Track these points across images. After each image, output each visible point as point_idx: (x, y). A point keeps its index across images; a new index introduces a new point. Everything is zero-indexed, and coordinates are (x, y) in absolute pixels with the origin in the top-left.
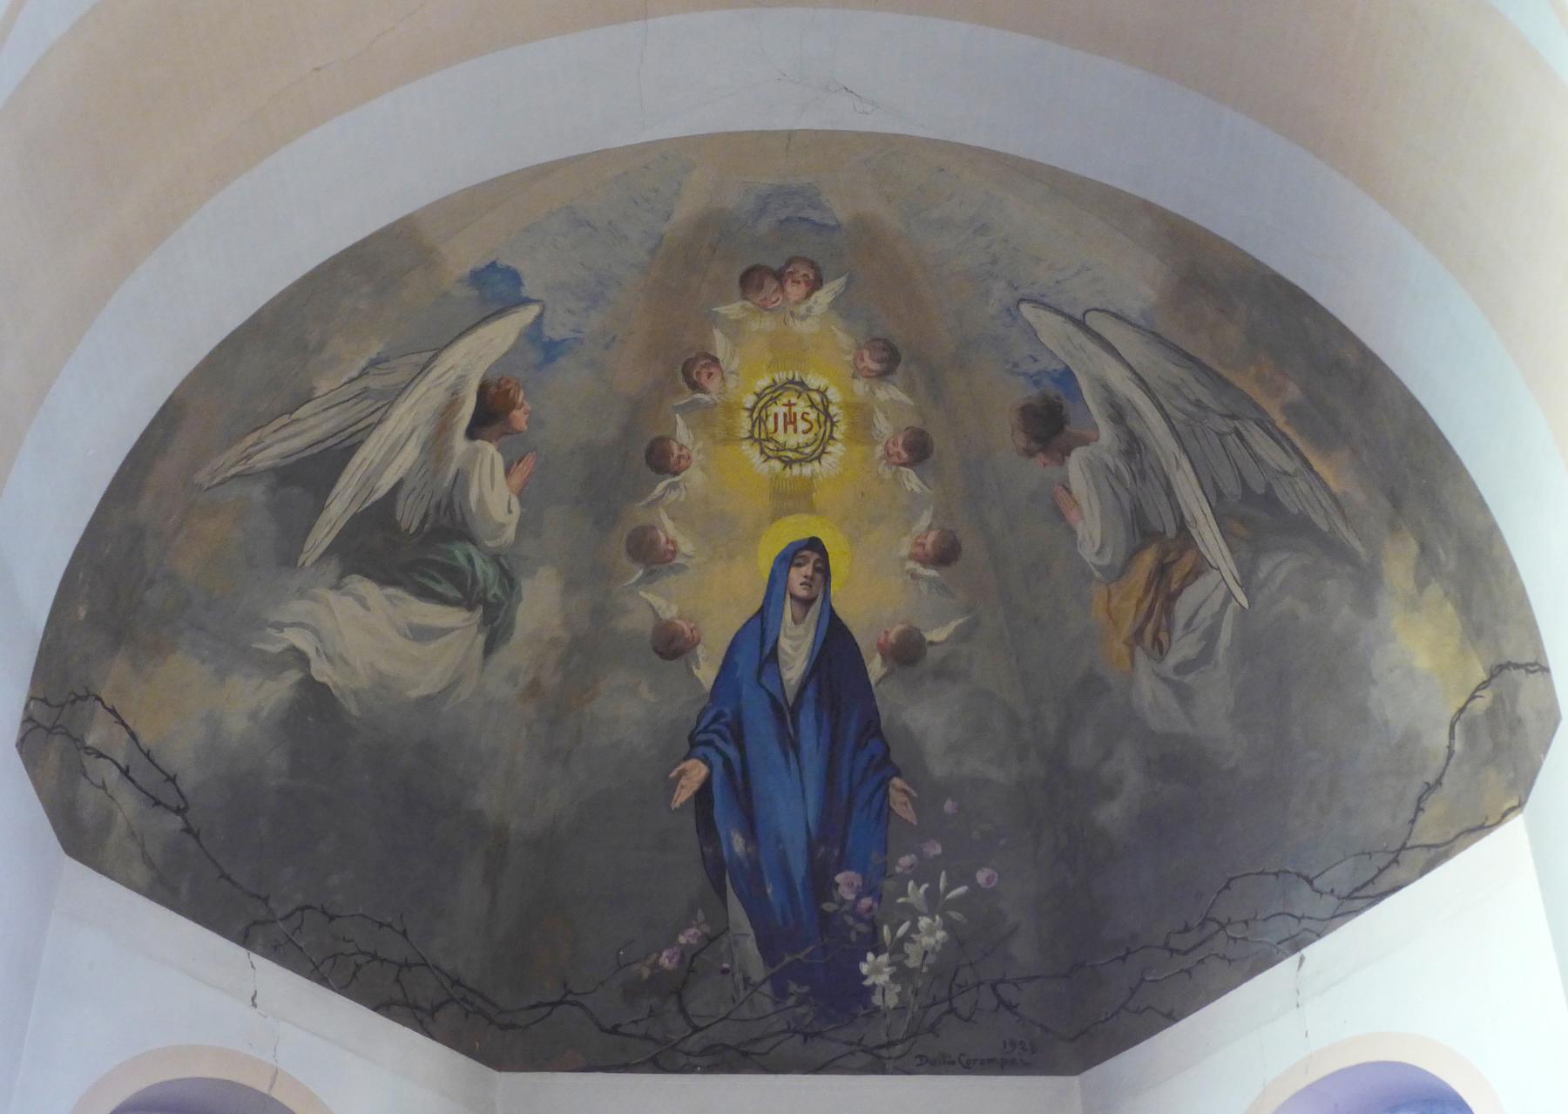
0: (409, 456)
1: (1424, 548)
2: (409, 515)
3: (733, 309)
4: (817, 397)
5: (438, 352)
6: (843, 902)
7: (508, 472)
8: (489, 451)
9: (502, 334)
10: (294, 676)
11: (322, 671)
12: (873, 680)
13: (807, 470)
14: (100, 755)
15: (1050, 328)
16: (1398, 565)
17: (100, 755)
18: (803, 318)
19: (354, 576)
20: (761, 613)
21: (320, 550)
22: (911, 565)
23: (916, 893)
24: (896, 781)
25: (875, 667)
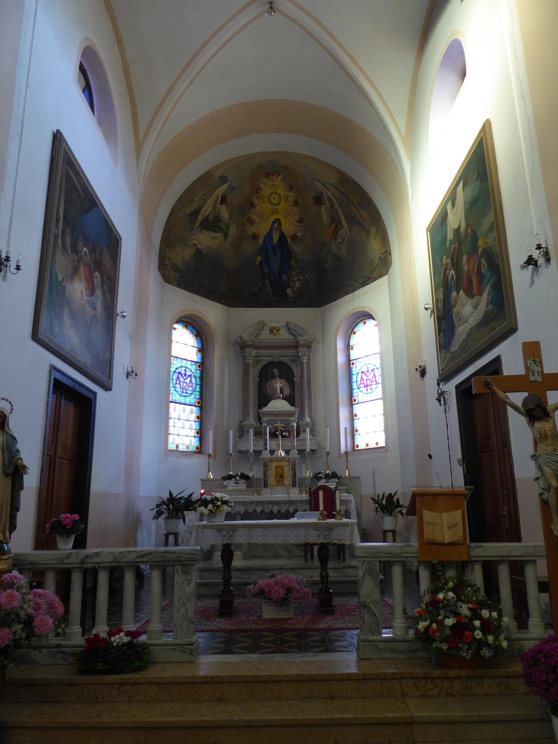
0: (210, 209)
1: (377, 229)
2: (211, 219)
3: (264, 180)
4: (279, 195)
5: (214, 191)
6: (284, 280)
7: (227, 210)
8: (223, 206)
9: (225, 187)
10: (195, 248)
11: (199, 247)
12: (289, 242)
13: (277, 207)
14: (167, 265)
15: (318, 185)
16: (373, 231)
17: (167, 265)
18: (276, 181)
19: (283, 380)
20: (270, 231)
21: (197, 227)
22: (295, 223)
23: (295, 278)
24: (292, 260)
25: (289, 240)
